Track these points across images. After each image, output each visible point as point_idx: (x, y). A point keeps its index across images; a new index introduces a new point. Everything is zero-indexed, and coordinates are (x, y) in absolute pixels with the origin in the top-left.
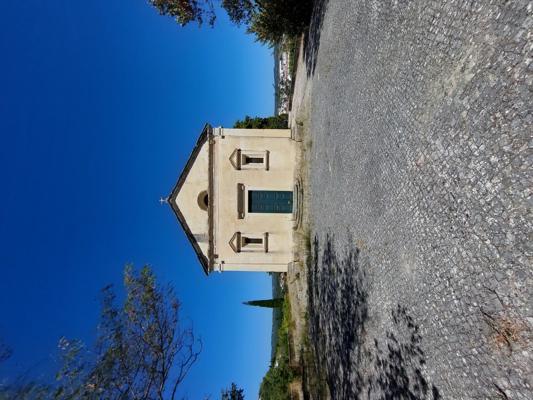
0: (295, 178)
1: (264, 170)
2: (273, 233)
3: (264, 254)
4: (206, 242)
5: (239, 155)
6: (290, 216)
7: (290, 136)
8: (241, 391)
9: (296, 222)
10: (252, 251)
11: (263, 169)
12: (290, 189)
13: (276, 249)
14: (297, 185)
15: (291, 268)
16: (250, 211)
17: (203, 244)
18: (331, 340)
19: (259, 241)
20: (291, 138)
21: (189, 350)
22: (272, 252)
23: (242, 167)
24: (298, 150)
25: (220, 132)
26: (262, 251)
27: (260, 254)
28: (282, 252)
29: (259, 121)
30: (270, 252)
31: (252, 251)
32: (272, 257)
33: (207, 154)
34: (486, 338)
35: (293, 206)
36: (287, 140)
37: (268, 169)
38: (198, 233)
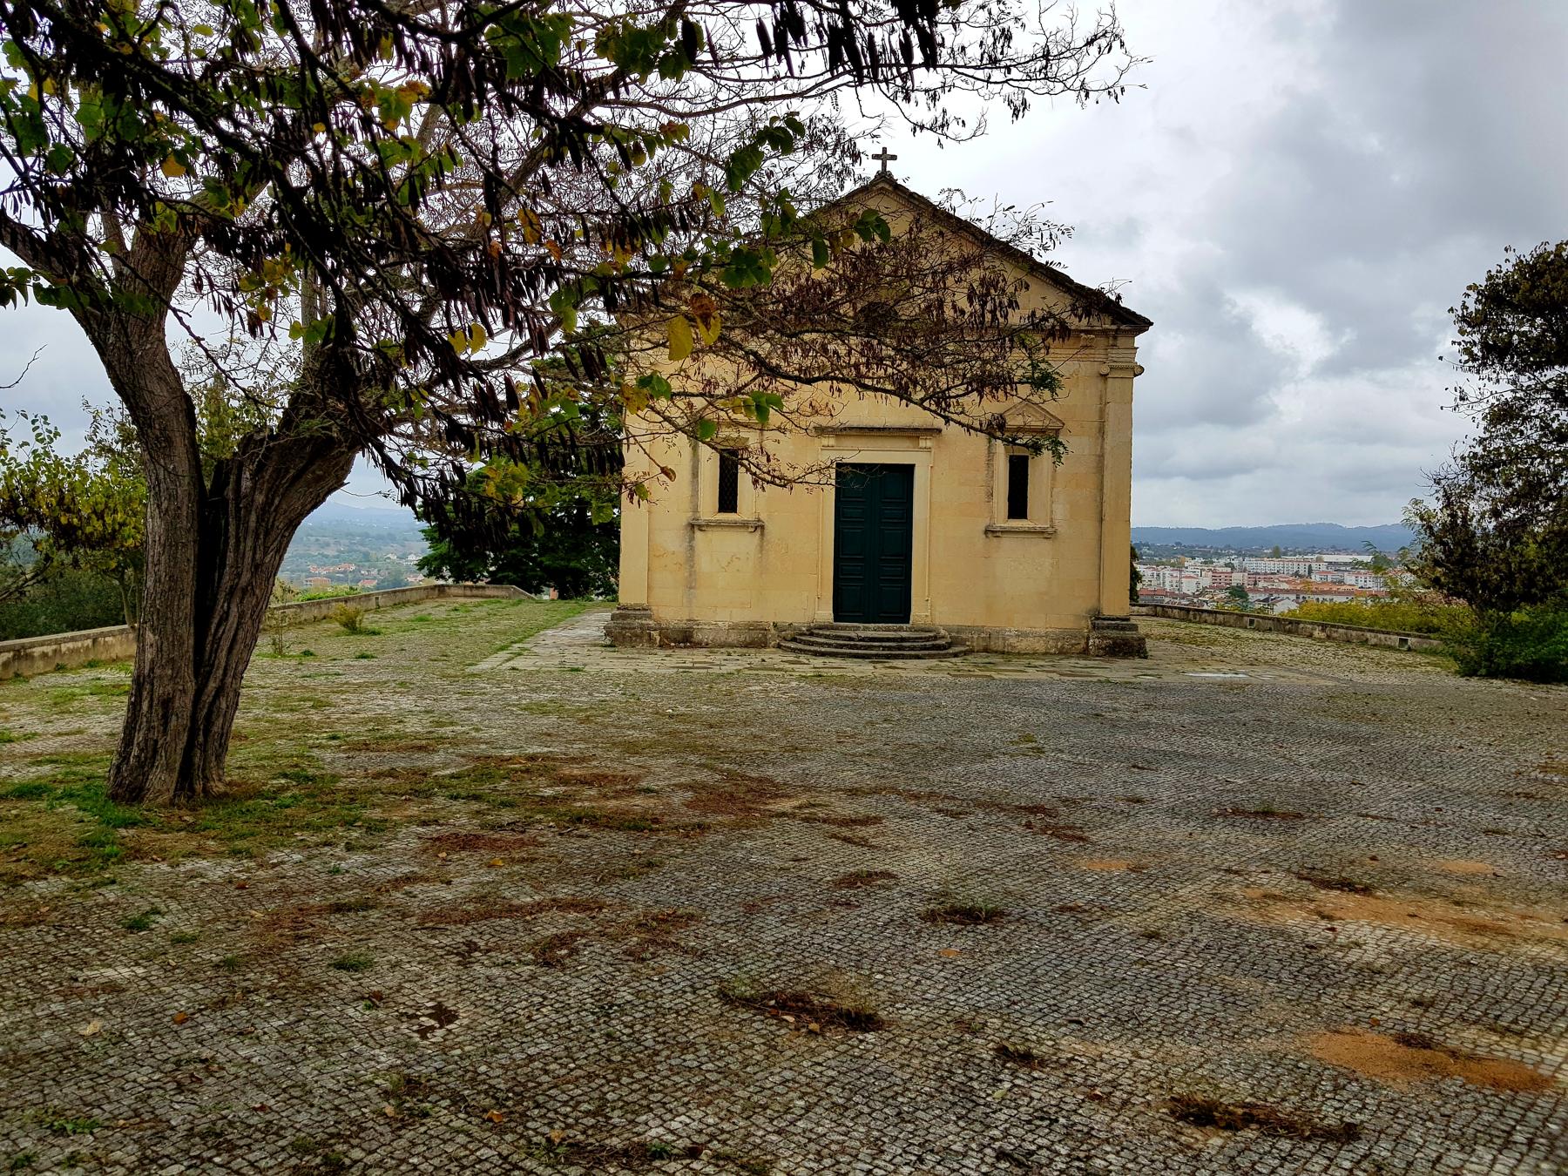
0: (960, 630)
1: (987, 522)
2: (761, 551)
3: (686, 517)
6: (826, 613)
7: (1106, 612)
12: (920, 611)
13: (704, 563)
14: (935, 638)
15: (636, 617)
18: (254, 553)
20: (1097, 619)
21: (986, 441)
22: (692, 548)
24: (1057, 640)
25: (1121, 369)
26: (695, 510)
28: (691, 584)
29: (1379, 566)
30: (692, 539)
34: (305, 1101)
35: (861, 625)
37: (987, 532)
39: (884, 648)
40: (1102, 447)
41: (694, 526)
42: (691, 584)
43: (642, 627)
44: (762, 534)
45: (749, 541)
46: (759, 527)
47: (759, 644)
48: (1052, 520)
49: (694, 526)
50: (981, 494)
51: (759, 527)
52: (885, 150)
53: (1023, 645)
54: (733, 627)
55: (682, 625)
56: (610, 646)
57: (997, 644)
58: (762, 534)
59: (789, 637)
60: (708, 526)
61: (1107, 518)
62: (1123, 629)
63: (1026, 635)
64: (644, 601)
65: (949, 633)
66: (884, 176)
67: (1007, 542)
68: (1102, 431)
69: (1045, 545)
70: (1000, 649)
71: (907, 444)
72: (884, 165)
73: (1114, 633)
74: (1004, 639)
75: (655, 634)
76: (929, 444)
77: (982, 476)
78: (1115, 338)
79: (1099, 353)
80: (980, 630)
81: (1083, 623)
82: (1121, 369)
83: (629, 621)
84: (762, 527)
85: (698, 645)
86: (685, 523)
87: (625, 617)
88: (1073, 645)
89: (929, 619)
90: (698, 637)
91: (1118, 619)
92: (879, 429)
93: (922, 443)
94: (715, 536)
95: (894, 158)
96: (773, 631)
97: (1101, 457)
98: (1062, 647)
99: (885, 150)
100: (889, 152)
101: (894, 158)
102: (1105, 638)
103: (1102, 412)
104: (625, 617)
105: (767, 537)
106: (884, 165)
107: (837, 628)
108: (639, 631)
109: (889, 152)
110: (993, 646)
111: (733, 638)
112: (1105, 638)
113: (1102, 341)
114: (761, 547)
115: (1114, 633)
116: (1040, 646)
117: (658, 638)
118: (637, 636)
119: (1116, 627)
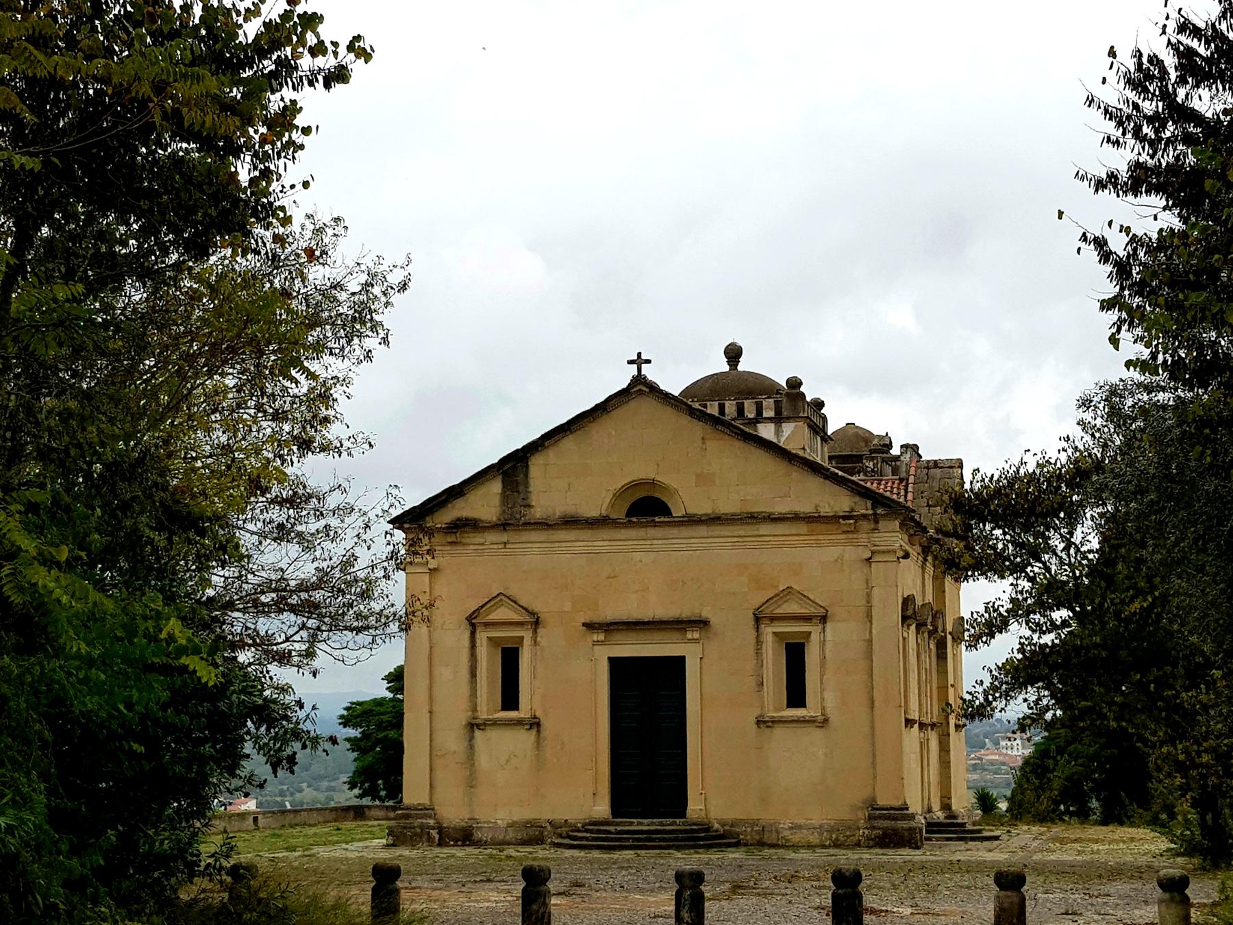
3: (463, 717)
4: (504, 512)
5: (807, 619)
6: (602, 809)
7: (881, 802)
8: (795, 383)
9: (579, 831)
10: (473, 674)
11: (762, 707)
12: (694, 807)
13: (483, 760)
16: (616, 664)
17: (497, 501)
19: (510, 699)
22: (471, 747)
23: (768, 631)
24: (830, 831)
25: (883, 552)
26: (474, 709)
27: (464, 704)
28: (471, 782)
30: (472, 738)
31: (473, 674)
32: (453, 748)
33: (806, 508)
35: (635, 820)
36: (865, 793)
38: (531, 482)
39: (634, 840)
40: (871, 632)
41: (473, 726)
42: (471, 782)
43: (422, 827)
44: (539, 732)
45: (525, 738)
46: (534, 724)
47: (537, 840)
48: (823, 708)
49: (473, 726)
50: (751, 682)
51: (534, 724)
52: (639, 355)
53: (796, 838)
54: (510, 825)
55: (463, 824)
56: (393, 845)
57: (770, 838)
58: (539, 732)
59: (564, 834)
60: (485, 724)
61: (876, 704)
62: (895, 819)
63: (800, 827)
64: (425, 800)
65: (723, 826)
66: (639, 380)
67: (779, 731)
68: (869, 616)
69: (816, 734)
70: (775, 842)
71: (676, 635)
72: (639, 370)
73: (886, 824)
74: (778, 832)
75: (434, 833)
76: (696, 635)
77: (751, 664)
78: (877, 522)
79: (863, 537)
80: (754, 823)
81: (860, 814)
82: (883, 552)
83: (411, 820)
84: (539, 724)
85: (478, 844)
86: (464, 723)
87: (407, 817)
88: (848, 837)
89: (703, 814)
90: (478, 835)
91: (892, 809)
92: (649, 623)
93: (689, 635)
94: (493, 734)
95: (648, 361)
96: (549, 828)
97: (870, 641)
98: (837, 839)
99: (639, 355)
100: (644, 357)
101: (648, 361)
102: (873, 828)
103: (869, 595)
104: (407, 817)
105: (542, 728)
106: (639, 370)
107: (618, 824)
108: (418, 830)
109: (644, 357)
110: (766, 839)
111: (511, 835)
112: (873, 828)
113: (865, 525)
114: (538, 744)
115: (886, 824)
116: (814, 839)
117: (437, 837)
118: (415, 834)
119: (889, 818)
